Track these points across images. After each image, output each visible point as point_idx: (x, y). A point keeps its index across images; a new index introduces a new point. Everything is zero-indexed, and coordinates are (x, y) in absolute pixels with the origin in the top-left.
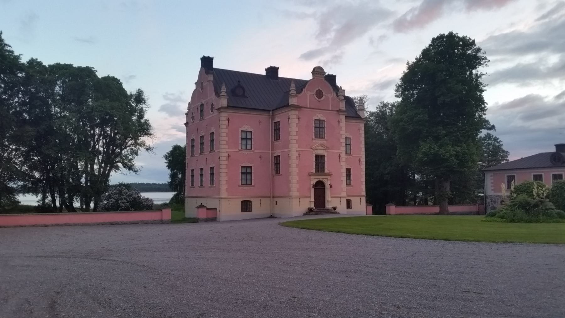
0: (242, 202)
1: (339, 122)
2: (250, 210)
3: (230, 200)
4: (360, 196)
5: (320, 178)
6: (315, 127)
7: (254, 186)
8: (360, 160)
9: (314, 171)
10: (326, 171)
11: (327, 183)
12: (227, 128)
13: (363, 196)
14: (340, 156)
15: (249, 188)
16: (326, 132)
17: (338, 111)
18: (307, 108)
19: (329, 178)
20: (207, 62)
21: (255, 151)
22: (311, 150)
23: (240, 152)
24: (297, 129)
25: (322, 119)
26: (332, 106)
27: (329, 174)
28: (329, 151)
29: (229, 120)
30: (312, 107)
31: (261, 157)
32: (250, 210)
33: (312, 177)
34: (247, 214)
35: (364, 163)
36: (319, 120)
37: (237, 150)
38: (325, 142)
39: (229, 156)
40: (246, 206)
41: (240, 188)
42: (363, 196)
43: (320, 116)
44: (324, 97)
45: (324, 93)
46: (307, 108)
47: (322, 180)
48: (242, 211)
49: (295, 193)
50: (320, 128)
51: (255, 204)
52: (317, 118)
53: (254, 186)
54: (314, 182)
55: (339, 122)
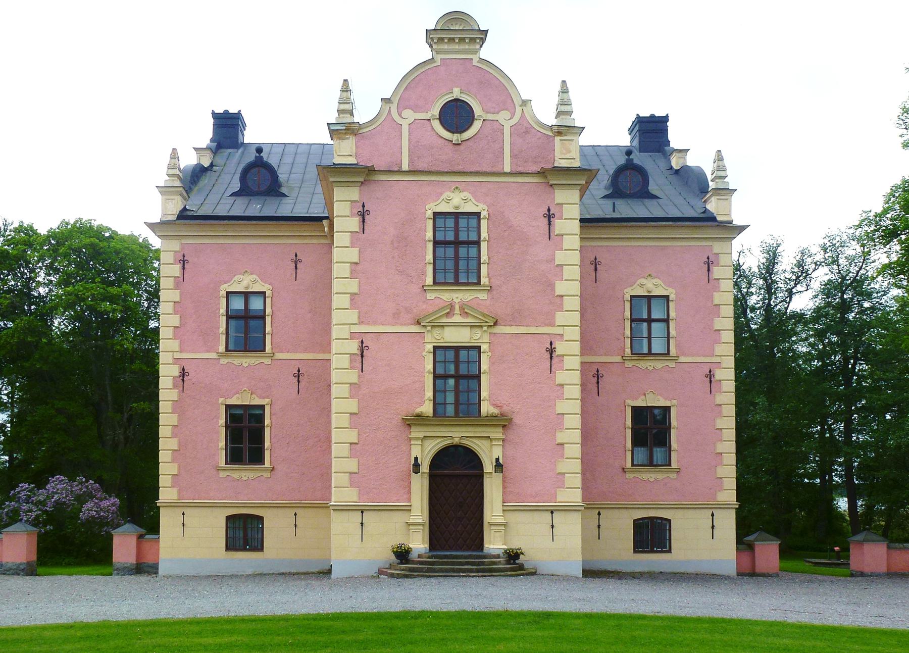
0: (229, 518)
1: (549, 217)
2: (259, 547)
3: (186, 511)
4: (714, 508)
5: (457, 435)
6: (436, 243)
7: (678, 471)
8: (710, 375)
9: (427, 408)
10: (486, 408)
11: (489, 453)
12: (177, 286)
13: (724, 507)
14: (551, 351)
15: (660, 476)
16: (484, 257)
17: (542, 173)
18: (400, 172)
19: (497, 433)
20: (228, 126)
21: (279, 356)
22: (416, 329)
23: (224, 361)
24: (353, 255)
25: (469, 208)
26: (513, 156)
27: (503, 421)
28: (498, 329)
29: (184, 262)
30: (421, 166)
31: (298, 375)
32: (259, 547)
33: (417, 432)
34: (245, 560)
35: (729, 386)
36: (457, 216)
37: (213, 355)
38: (483, 296)
39: (183, 373)
40: (244, 532)
41: (223, 474)
42: (724, 507)
43: (456, 199)
44: (477, 125)
45: (478, 111)
46: (400, 172)
47: (465, 442)
48: (228, 548)
49: (342, 493)
50: (457, 243)
51: (276, 528)
52: (444, 208)
53: (678, 471)
54: (425, 450)
55: (549, 217)
